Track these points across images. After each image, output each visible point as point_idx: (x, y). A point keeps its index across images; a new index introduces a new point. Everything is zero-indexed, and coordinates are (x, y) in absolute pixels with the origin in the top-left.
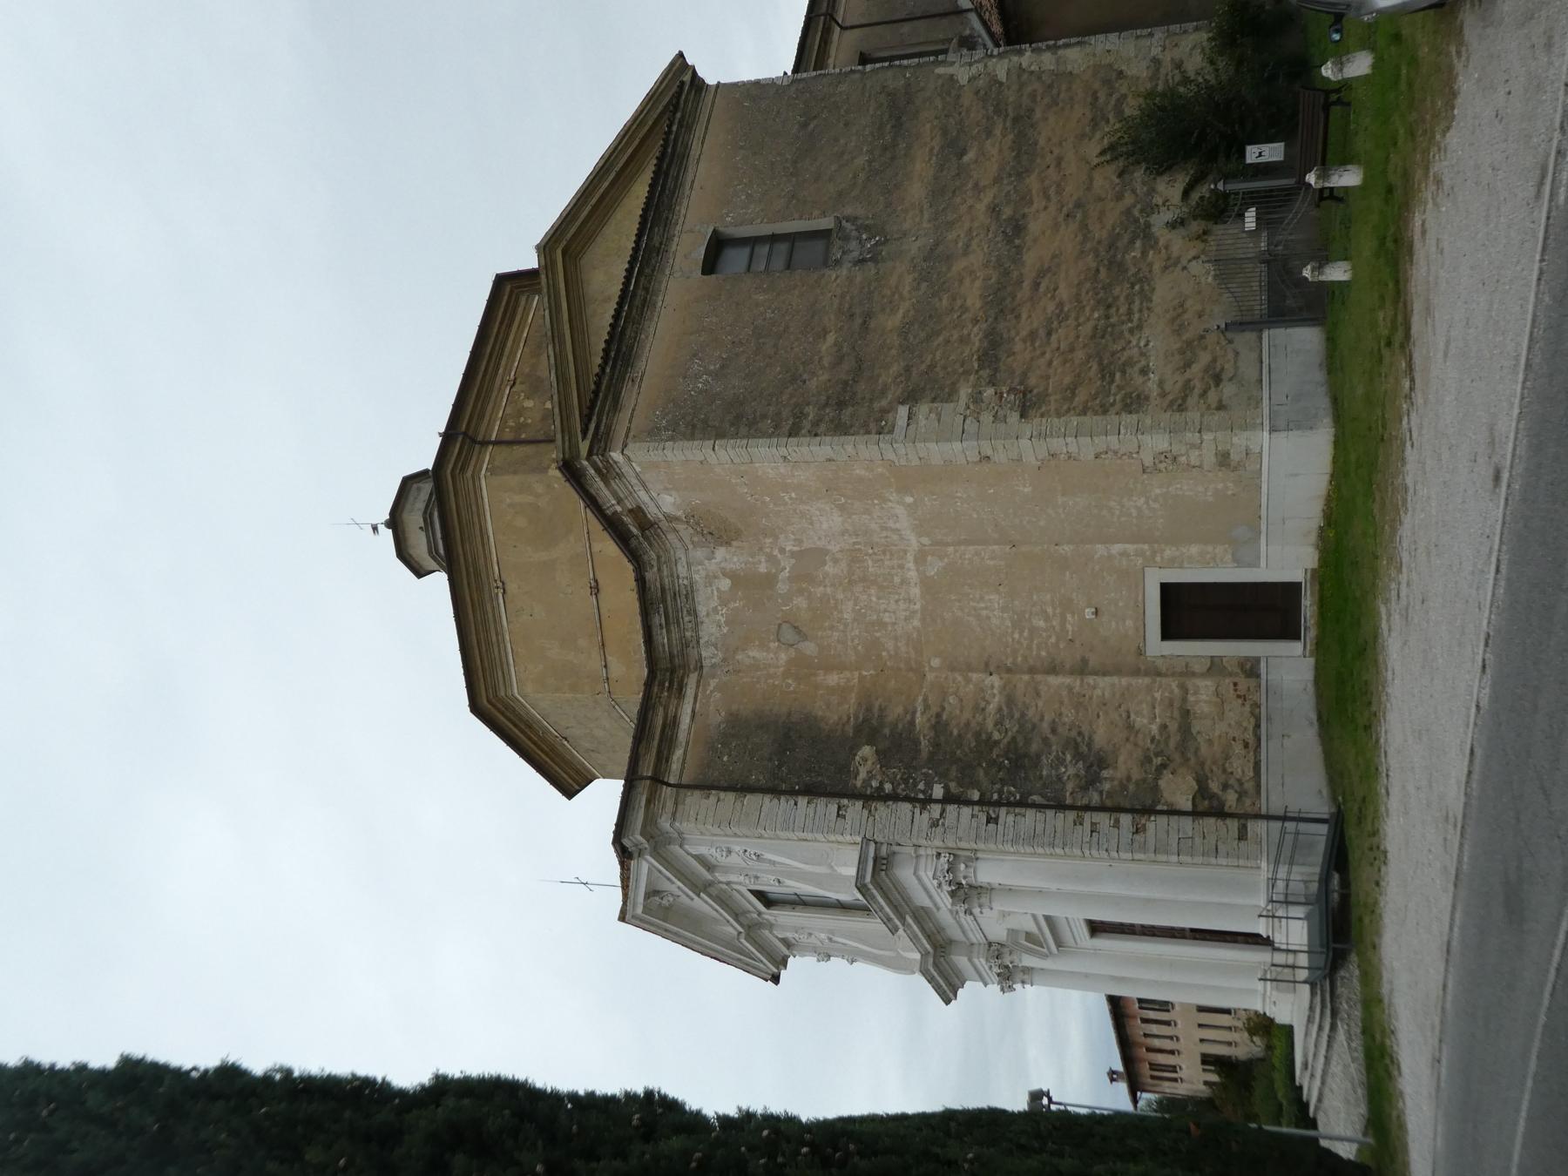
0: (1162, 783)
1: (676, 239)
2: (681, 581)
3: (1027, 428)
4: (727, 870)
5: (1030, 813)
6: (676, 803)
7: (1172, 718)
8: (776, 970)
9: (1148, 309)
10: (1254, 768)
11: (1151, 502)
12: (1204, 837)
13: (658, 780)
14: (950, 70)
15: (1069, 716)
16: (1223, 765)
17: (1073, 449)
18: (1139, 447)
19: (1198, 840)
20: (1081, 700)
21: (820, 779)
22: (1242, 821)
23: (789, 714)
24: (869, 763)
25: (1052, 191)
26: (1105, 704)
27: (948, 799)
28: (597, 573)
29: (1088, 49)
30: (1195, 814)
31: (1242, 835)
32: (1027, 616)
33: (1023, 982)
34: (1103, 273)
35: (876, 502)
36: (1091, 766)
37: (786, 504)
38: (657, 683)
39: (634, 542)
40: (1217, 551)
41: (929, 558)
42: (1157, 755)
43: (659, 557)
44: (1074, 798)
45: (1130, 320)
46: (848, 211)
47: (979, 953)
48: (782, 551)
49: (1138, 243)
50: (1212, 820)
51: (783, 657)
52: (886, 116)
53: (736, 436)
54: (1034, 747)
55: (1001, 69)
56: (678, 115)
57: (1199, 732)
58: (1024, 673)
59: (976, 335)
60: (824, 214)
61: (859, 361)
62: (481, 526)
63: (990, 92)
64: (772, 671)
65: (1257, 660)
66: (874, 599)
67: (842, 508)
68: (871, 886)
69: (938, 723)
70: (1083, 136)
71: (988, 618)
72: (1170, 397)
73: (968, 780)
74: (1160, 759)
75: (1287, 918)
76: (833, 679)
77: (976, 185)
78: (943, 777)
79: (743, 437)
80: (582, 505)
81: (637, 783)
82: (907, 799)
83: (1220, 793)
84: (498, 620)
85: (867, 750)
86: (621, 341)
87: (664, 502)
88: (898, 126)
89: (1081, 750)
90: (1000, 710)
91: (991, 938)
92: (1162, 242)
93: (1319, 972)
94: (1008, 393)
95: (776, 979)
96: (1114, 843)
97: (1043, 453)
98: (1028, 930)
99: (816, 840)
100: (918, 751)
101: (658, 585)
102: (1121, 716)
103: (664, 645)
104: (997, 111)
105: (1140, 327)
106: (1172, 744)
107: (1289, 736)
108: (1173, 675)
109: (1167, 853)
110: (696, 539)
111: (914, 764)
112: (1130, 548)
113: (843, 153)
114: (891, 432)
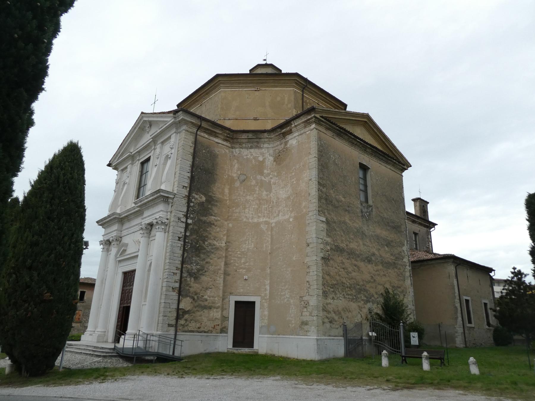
0: (188, 298)
1: (367, 156)
2: (262, 145)
3: (319, 259)
4: (161, 148)
5: (181, 252)
6: (191, 132)
7: (209, 303)
8: (113, 165)
9: (349, 300)
10: (191, 330)
11: (287, 299)
12: (170, 312)
13: (199, 127)
14: (406, 245)
15: (211, 268)
16: (193, 320)
17: (311, 274)
18: (311, 296)
19: (169, 310)
20: (216, 273)
21: (196, 182)
22: (174, 326)
23: (217, 175)
24: (200, 199)
25: (378, 273)
26: (214, 281)
27: (187, 224)
28: (261, 120)
29: (410, 286)
30: (178, 309)
31: (170, 325)
32: (245, 257)
33: (103, 248)
34: (358, 287)
35: (291, 209)
36: (195, 275)
37: (291, 180)
38: (229, 132)
39: (279, 130)
40: (266, 321)
41: (267, 226)
42: (198, 297)
43: (271, 138)
44: (185, 268)
45: (346, 295)
46: (374, 210)
47: (118, 233)
48: (271, 178)
49: (365, 298)
50: (175, 315)
51: (235, 175)
52: (396, 224)
53: (319, 165)
54: (202, 256)
55: (406, 260)
56: (397, 163)
57: (204, 312)
58: (225, 254)
59: (343, 245)
60: (373, 202)
61: (337, 207)
62: (277, 86)
63: (399, 257)
64: (230, 171)
65: (227, 333)
66: (253, 207)
67: (288, 198)
68: (158, 195)
69: (211, 224)
70: (391, 283)
71: (245, 244)
72: (326, 307)
73: (193, 231)
74: (196, 298)
75: (134, 340)
76: (227, 191)
77: (380, 249)
78: (194, 224)
79: (318, 167)
80: (288, 118)
81: (199, 120)
82: (188, 210)
83: (184, 318)
84: (246, 87)
85: (204, 199)
86: (344, 134)
87: (293, 141)
88: (394, 228)
89: (200, 271)
90: (214, 245)
91: (123, 238)
92: (365, 306)
93: (122, 352)
94: (328, 254)
95: (109, 165)
96: (170, 280)
97: (309, 264)
98: (127, 250)
99: (175, 177)
100: (203, 216)
101: (262, 137)
102: (210, 286)
103: (241, 136)
104: (396, 258)
105: (345, 297)
106: (201, 303)
107: (201, 343)
108: (223, 304)
109: (165, 299)
110: (277, 151)
111: (199, 214)
112: (268, 292)
113: (387, 210)
114: (319, 215)
